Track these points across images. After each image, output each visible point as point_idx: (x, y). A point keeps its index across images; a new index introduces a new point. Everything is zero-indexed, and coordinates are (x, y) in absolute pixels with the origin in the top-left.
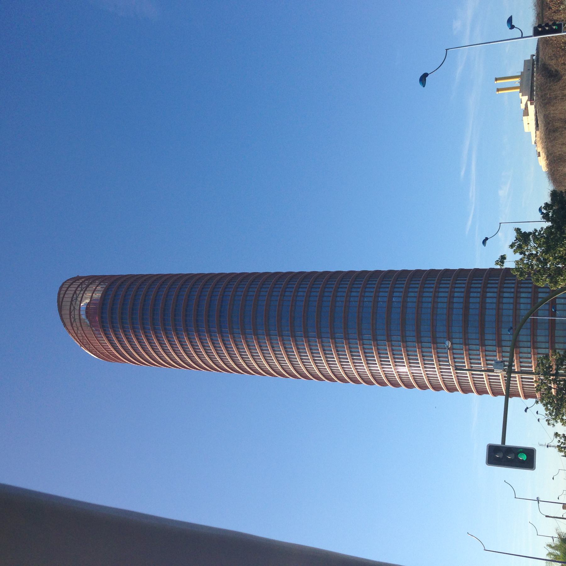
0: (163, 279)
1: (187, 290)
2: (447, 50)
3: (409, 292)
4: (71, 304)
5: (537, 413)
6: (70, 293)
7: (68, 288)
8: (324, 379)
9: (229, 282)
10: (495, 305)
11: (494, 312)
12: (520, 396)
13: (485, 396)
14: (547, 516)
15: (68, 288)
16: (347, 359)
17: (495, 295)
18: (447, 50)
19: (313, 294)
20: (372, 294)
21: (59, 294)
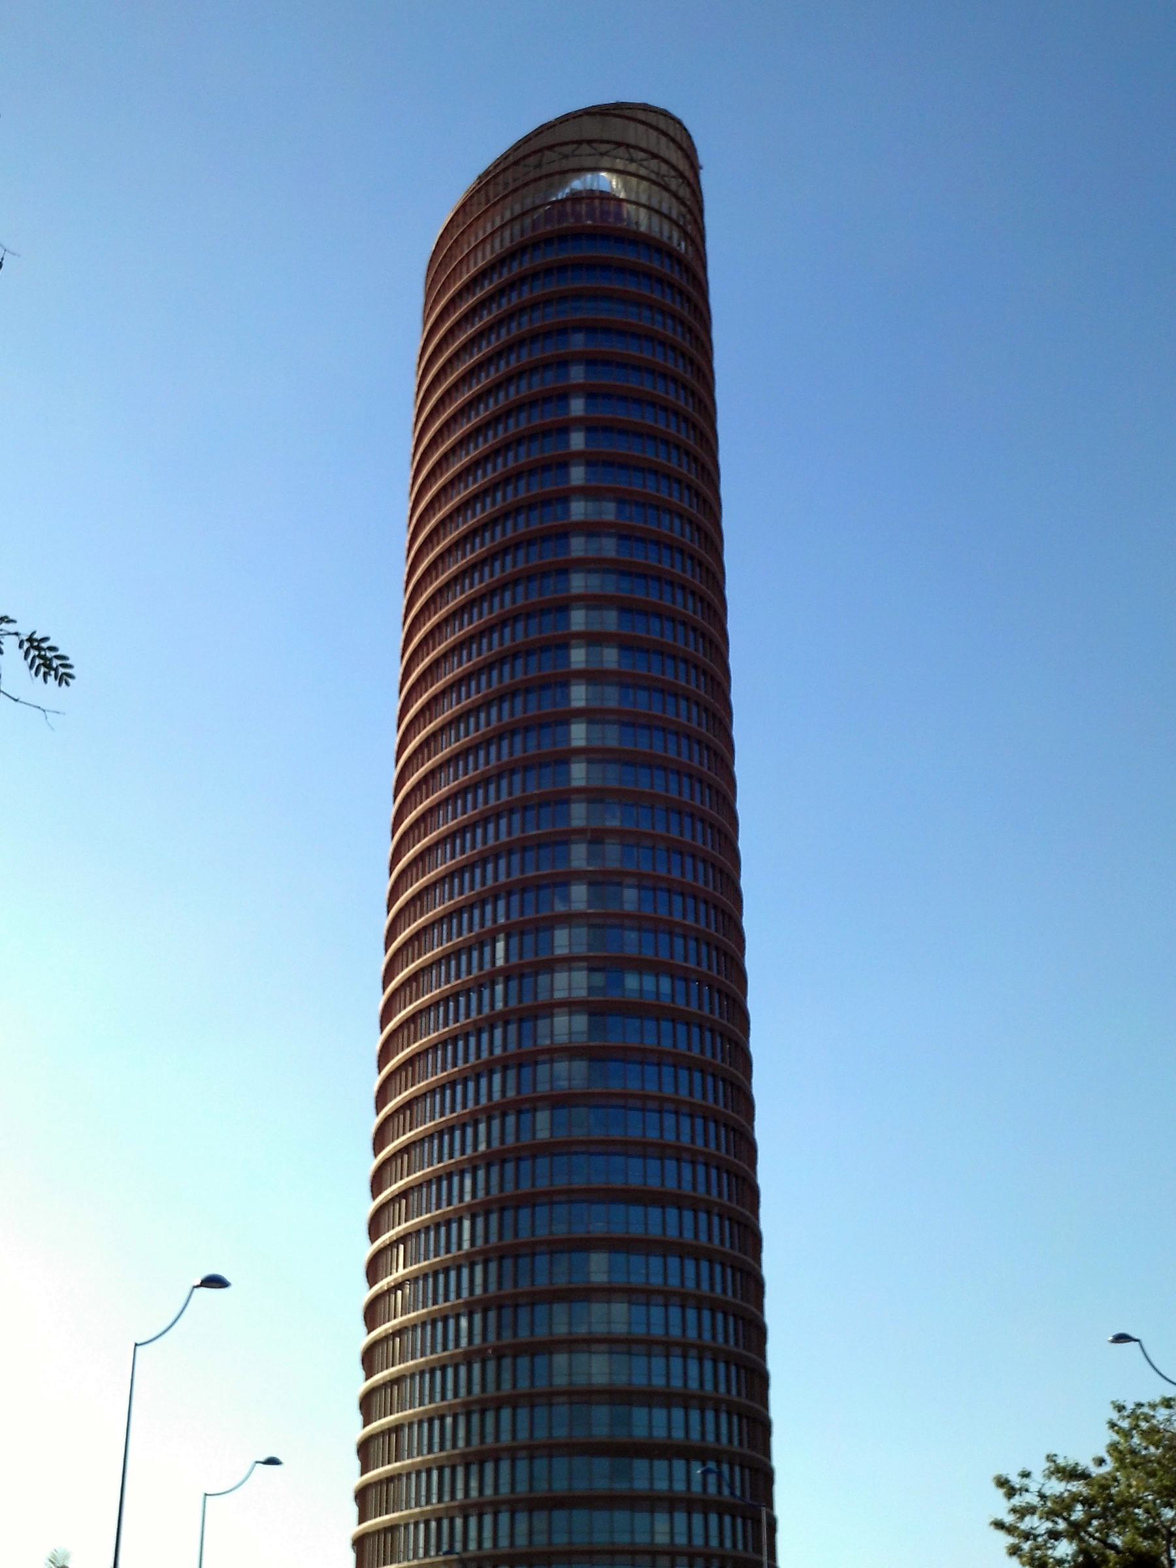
0: (694, 293)
1: (668, 301)
2: (136, 1345)
3: (689, 1514)
4: (619, 144)
5: (214, 1282)
6: (650, 140)
7: (665, 134)
8: (381, 1198)
9: (705, 673)
10: (642, 1279)
11: (623, 1539)
12: (362, 1473)
13: (353, 1510)
14: (16, 700)
15: (665, 134)
16: (449, 939)
17: (698, 1541)
18: (136, 1345)
19: (679, 942)
20: (684, 1093)
21: (645, 108)
